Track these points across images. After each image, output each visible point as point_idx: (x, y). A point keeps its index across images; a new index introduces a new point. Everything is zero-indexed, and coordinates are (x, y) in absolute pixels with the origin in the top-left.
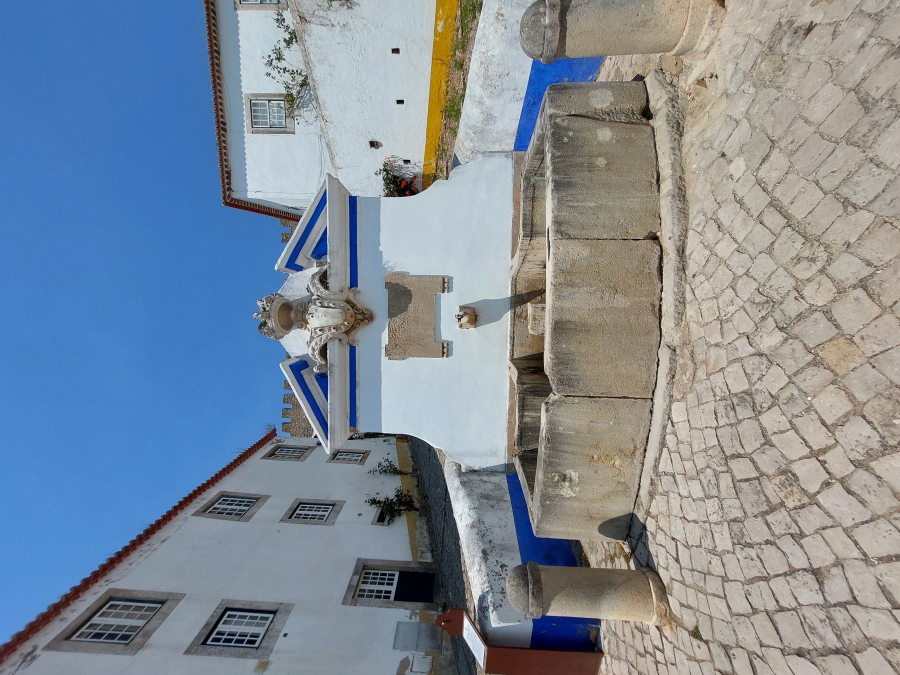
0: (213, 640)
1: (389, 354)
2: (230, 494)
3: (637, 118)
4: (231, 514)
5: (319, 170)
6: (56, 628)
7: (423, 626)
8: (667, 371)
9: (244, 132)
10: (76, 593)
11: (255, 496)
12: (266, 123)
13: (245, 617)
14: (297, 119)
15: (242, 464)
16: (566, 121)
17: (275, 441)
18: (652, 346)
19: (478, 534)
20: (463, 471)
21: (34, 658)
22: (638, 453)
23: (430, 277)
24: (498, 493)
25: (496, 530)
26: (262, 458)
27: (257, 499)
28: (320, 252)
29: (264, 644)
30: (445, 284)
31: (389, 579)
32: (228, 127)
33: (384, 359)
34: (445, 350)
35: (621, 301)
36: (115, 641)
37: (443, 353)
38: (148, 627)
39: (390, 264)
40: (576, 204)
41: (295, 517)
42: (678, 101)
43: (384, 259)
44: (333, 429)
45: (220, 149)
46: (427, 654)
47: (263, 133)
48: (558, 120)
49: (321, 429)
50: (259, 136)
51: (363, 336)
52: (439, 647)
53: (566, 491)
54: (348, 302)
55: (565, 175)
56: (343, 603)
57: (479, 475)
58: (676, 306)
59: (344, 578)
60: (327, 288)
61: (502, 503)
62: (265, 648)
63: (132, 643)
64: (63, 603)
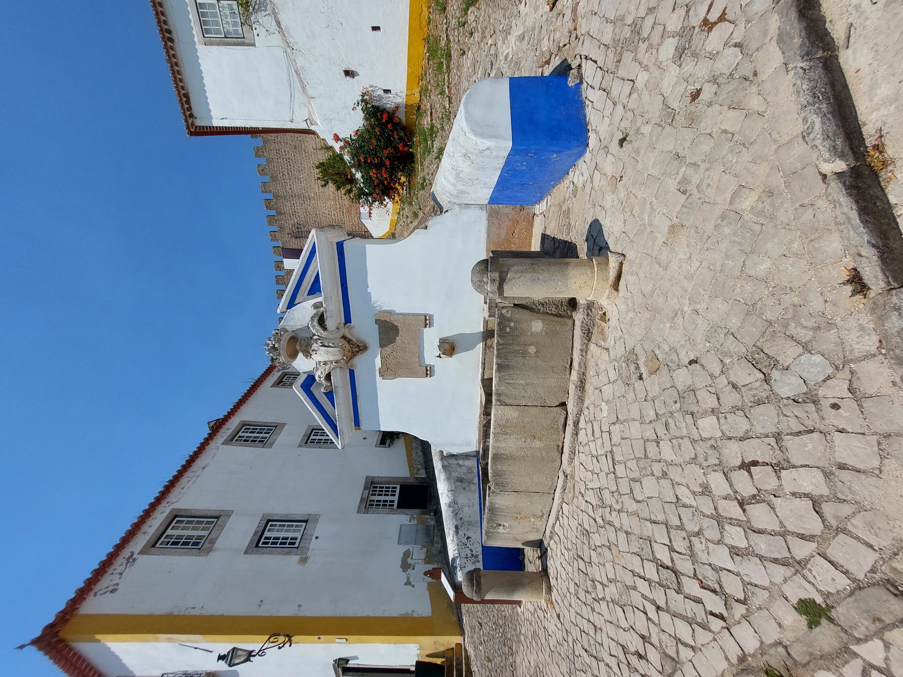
0: (263, 544)
1: (382, 375)
2: (250, 423)
3: (564, 310)
4: (256, 441)
5: (289, 93)
6: (141, 541)
7: (420, 526)
8: (561, 486)
9: (195, 44)
10: (147, 514)
11: (273, 425)
12: (218, 32)
13: (284, 526)
14: (256, 29)
15: (255, 393)
16: (510, 312)
17: (281, 368)
18: (555, 468)
19: (453, 512)
20: (445, 455)
21: (134, 560)
22: (545, 516)
23: (414, 315)
24: (469, 476)
25: (466, 509)
26: (271, 387)
27: (276, 427)
28: (315, 289)
29: (302, 545)
30: (427, 321)
31: (392, 491)
32: (174, 36)
33: (379, 379)
34: (428, 372)
35: (537, 444)
36: (189, 547)
37: (427, 374)
38: (213, 536)
39: (378, 303)
40: (511, 382)
41: (310, 442)
42: (593, 310)
43: (372, 299)
44: (342, 432)
45: (172, 66)
46: (423, 547)
47: (218, 44)
48: (504, 311)
49: (332, 431)
50: (214, 49)
51: (360, 362)
52: (432, 542)
53: (501, 530)
54: (344, 337)
55: (505, 359)
56: (358, 512)
57: (456, 459)
58: (569, 454)
59: (357, 492)
60: (325, 329)
61: (472, 486)
62: (304, 547)
63: (203, 547)
64: (140, 522)
